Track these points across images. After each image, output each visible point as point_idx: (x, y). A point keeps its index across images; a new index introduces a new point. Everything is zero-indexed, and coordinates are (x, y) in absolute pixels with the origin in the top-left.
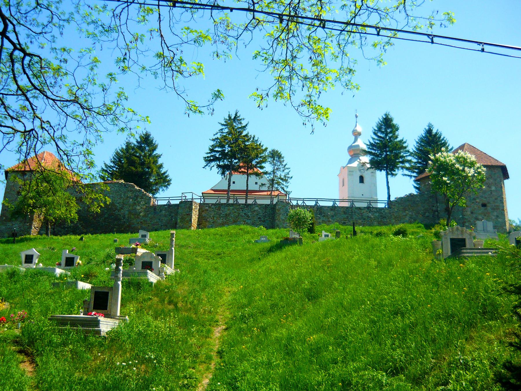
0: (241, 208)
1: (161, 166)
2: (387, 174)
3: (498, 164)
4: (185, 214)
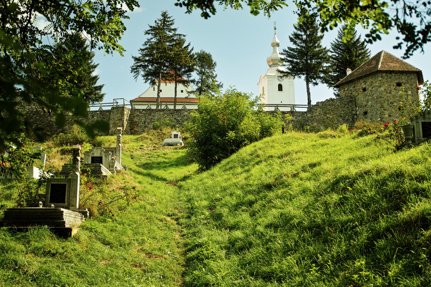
0: (172, 113)
1: (95, 79)
2: (308, 81)
3: (413, 70)
4: (116, 119)
